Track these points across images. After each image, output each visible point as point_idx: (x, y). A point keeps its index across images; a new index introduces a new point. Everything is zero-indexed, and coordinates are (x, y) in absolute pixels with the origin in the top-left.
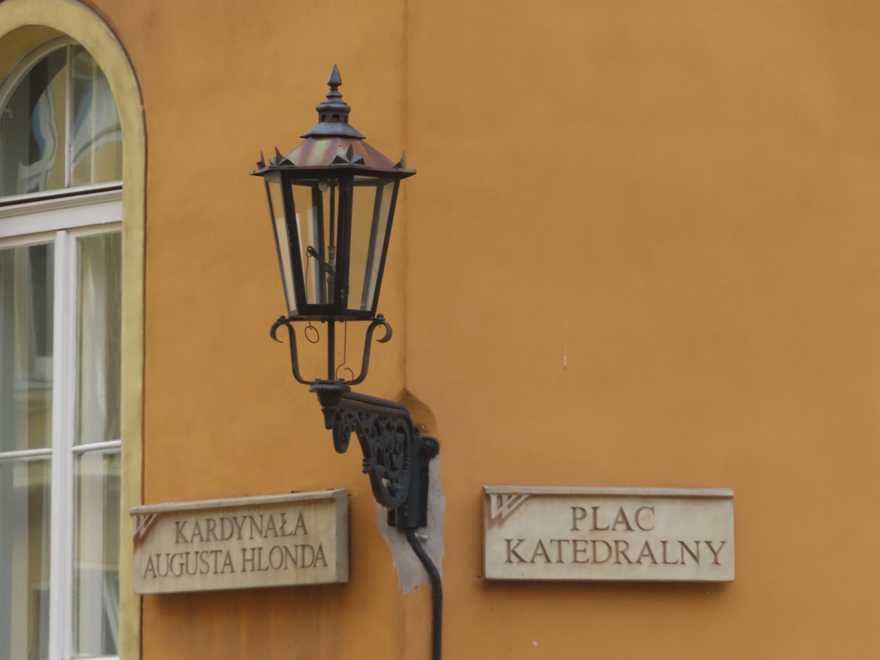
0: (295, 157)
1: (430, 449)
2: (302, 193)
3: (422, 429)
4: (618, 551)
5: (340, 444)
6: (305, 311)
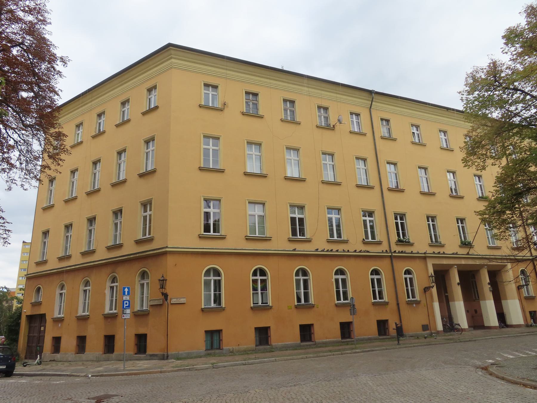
0: (160, 279)
1: (168, 296)
2: (161, 281)
3: (493, 211)
4: (179, 301)
5: (163, 296)
6: (161, 288)
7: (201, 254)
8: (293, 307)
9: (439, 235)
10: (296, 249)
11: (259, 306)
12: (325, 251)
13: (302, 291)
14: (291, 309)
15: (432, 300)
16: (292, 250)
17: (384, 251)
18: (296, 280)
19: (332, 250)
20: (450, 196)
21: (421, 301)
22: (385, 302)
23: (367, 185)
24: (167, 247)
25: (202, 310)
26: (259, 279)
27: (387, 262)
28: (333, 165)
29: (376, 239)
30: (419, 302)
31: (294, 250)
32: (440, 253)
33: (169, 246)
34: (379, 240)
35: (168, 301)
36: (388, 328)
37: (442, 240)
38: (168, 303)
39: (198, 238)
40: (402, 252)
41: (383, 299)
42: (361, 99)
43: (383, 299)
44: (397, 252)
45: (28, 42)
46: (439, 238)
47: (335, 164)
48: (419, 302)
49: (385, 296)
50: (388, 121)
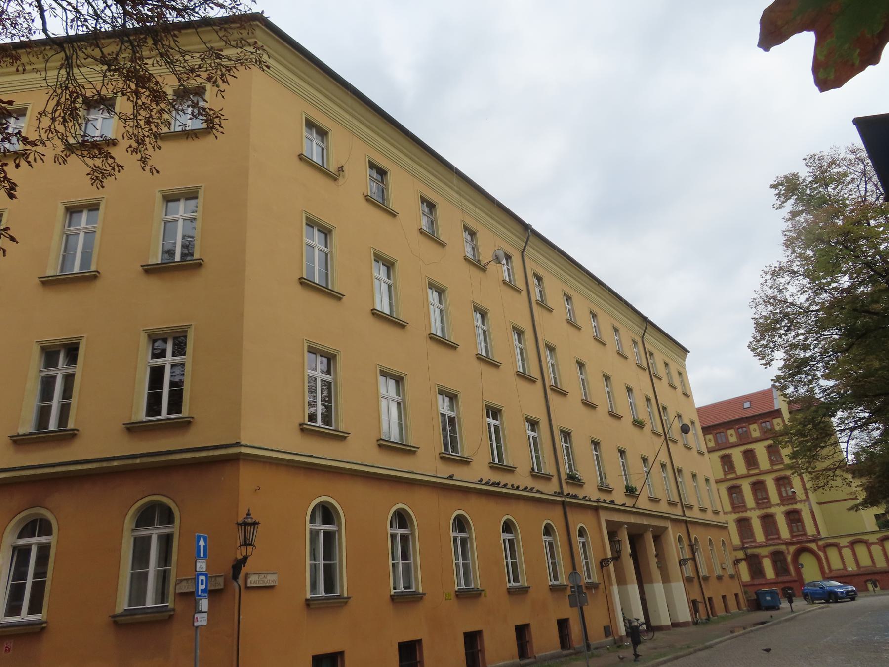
7: (305, 468)
8: (453, 595)
9: (605, 474)
10: (625, 504)
11: (462, 590)
12: (483, 482)
13: (321, 562)
14: (451, 599)
15: (611, 584)
16: (476, 481)
17: (509, 486)
18: (311, 531)
19: (532, 489)
20: (610, 414)
21: (425, 594)
22: (339, 597)
23: (325, 286)
24: (238, 444)
25: (308, 603)
26: (398, 533)
27: (558, 512)
28: (327, 255)
29: (459, 453)
30: (345, 600)
31: (451, 477)
32: (507, 487)
33: (243, 443)
34: (548, 473)
35: (241, 580)
36: (568, 635)
37: (342, 423)
38: (239, 585)
39: (298, 432)
40: (497, 484)
41: (519, 582)
42: (512, 233)
43: (519, 582)
44: (509, 486)
45: (174, 14)
46: (605, 478)
47: (331, 252)
48: (345, 600)
49: (561, 572)
50: (382, 173)
